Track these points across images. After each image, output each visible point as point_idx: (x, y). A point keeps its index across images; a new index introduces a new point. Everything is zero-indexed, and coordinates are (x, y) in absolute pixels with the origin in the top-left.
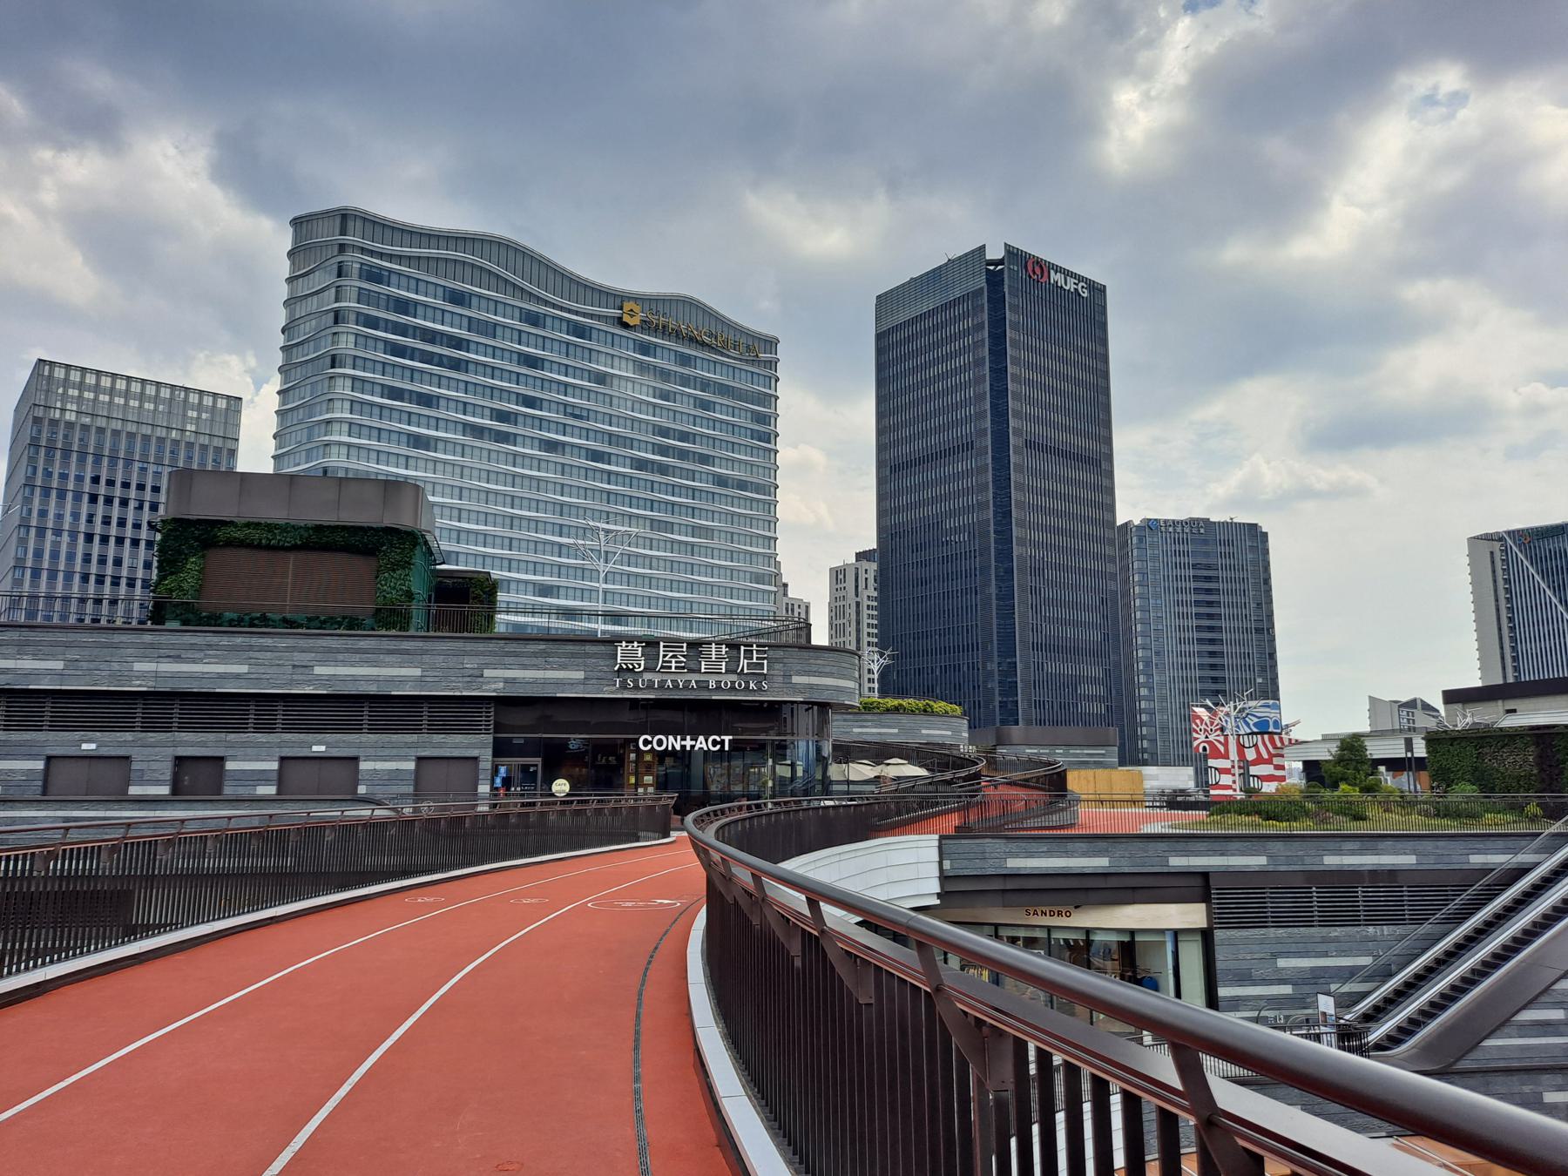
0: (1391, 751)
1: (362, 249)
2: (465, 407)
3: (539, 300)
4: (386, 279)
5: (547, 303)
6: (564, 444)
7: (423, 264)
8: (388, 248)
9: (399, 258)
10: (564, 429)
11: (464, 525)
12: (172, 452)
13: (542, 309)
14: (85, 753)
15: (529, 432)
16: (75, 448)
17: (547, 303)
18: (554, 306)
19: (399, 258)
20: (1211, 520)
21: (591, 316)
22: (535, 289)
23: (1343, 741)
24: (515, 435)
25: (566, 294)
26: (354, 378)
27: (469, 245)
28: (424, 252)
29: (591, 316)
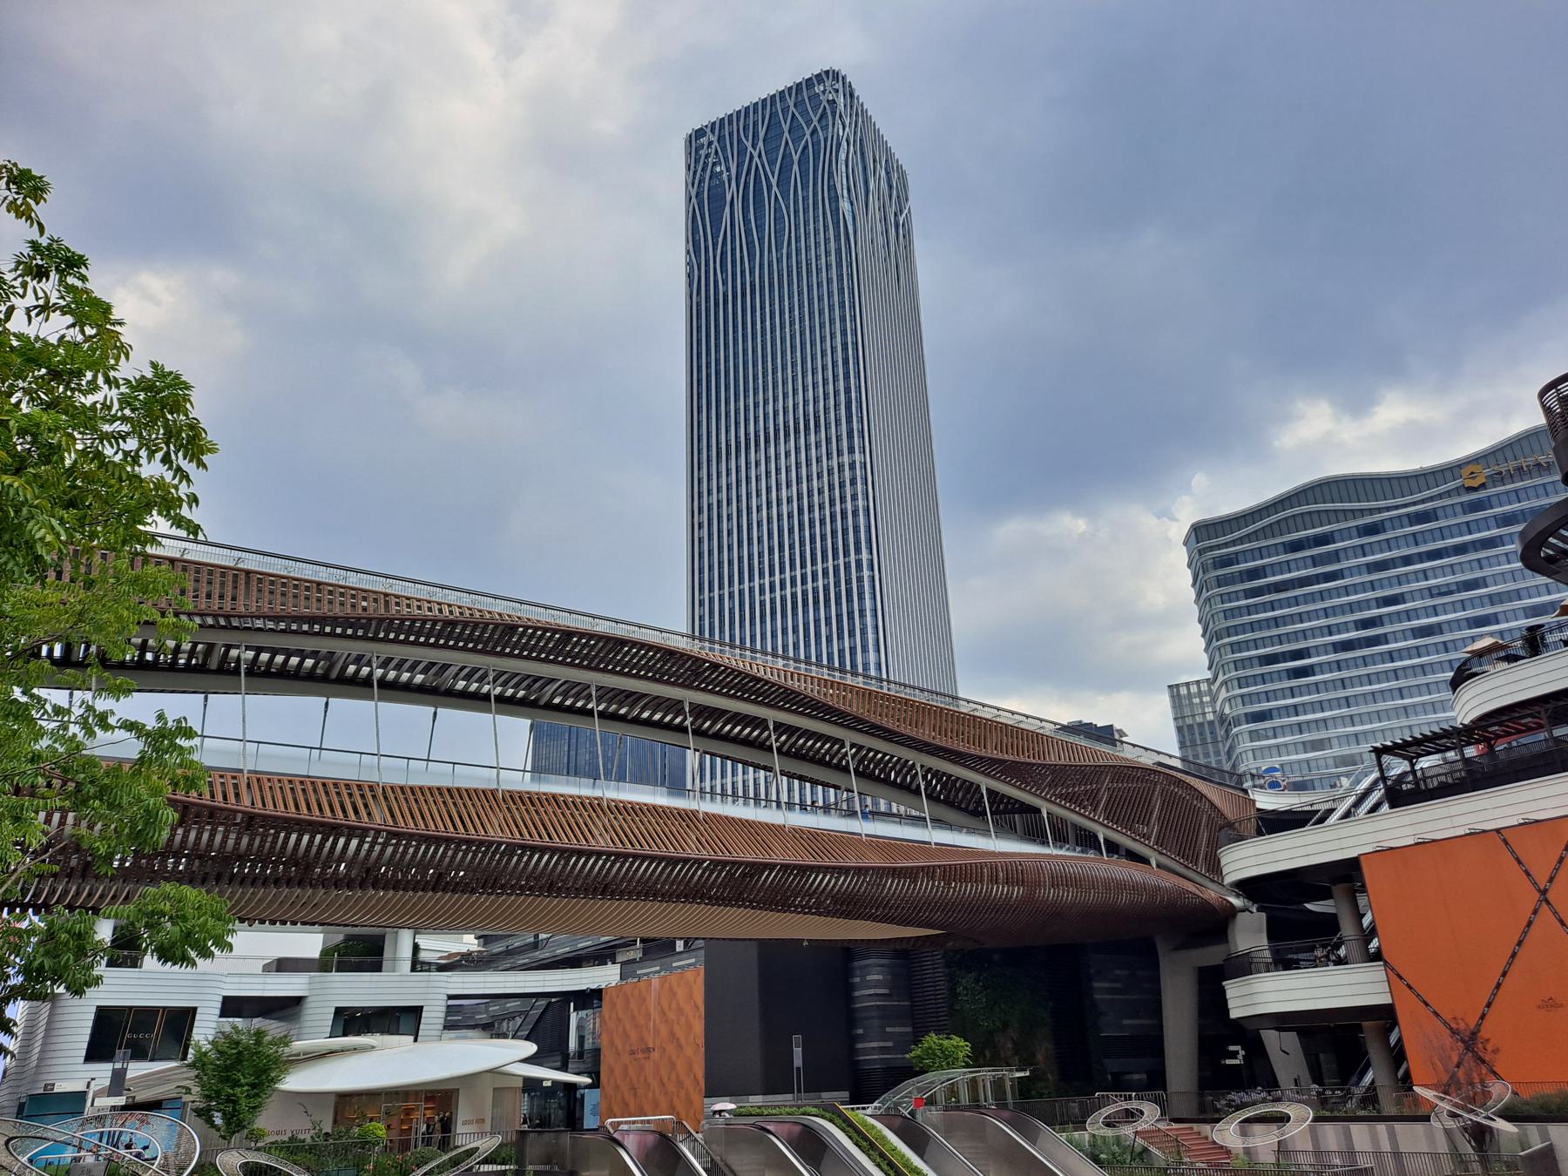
0: (131, 996)
1: (1211, 547)
2: (1330, 630)
3: (1371, 511)
4: (1235, 560)
5: (1380, 510)
6: (1439, 625)
7: (1261, 534)
8: (1222, 540)
9: (1241, 540)
10: (1435, 611)
11: (1359, 728)
12: (1211, 733)
13: (1377, 517)
14: (655, 962)
15: (1398, 627)
16: (1210, 745)
17: (1380, 510)
18: (1388, 509)
19: (1241, 540)
20: (33, 173)
21: (1431, 499)
22: (1364, 505)
23: (1546, 646)
24: (1385, 635)
25: (1362, 496)
26: (1231, 644)
27: (1287, 503)
28: (1252, 528)
29: (1431, 499)
